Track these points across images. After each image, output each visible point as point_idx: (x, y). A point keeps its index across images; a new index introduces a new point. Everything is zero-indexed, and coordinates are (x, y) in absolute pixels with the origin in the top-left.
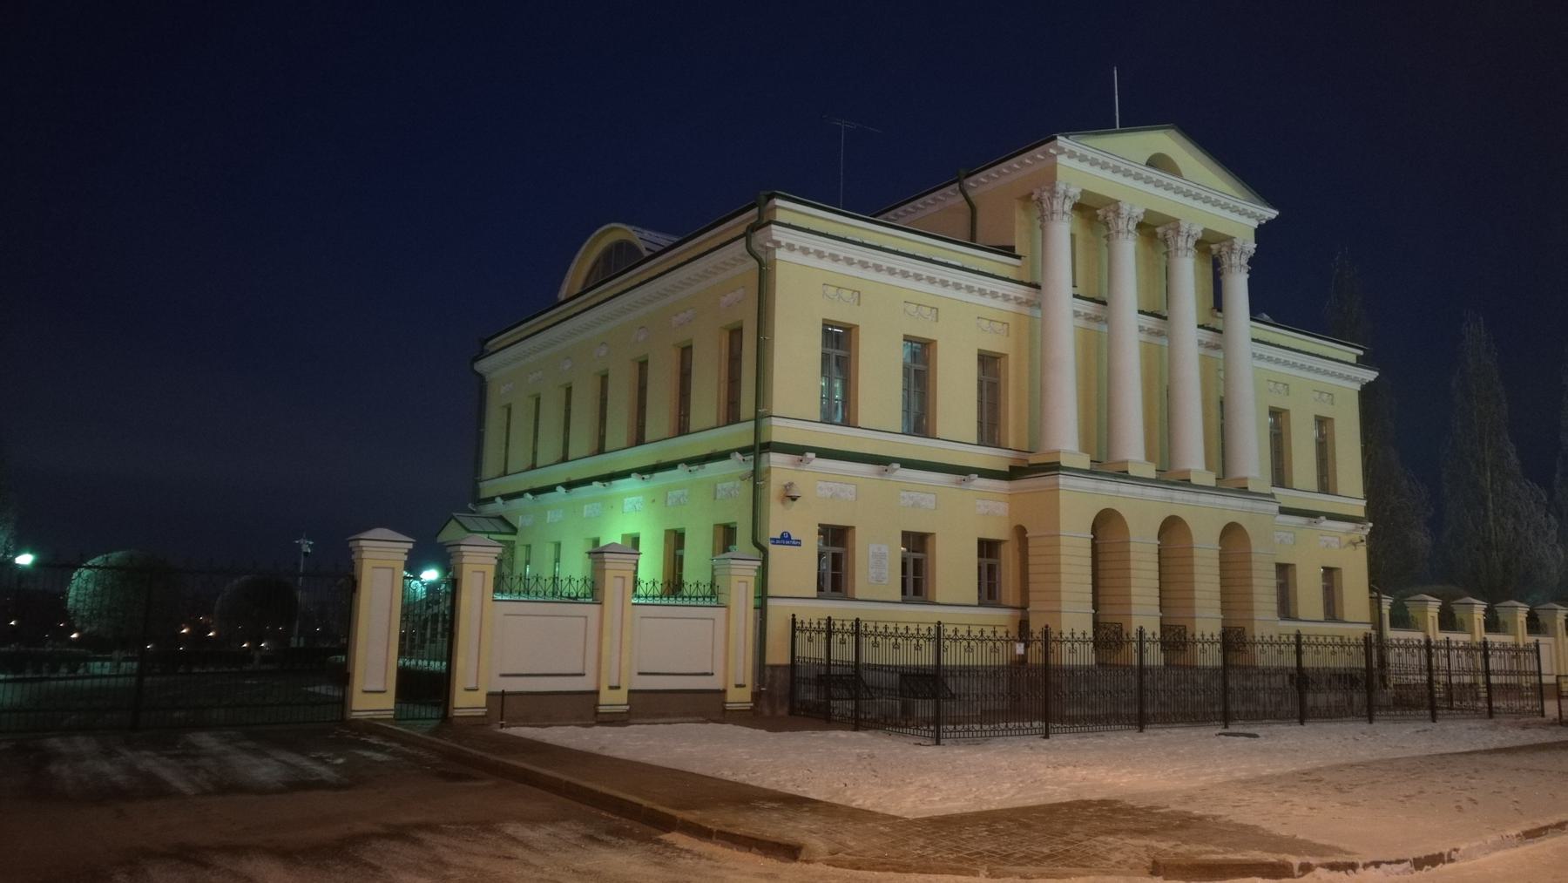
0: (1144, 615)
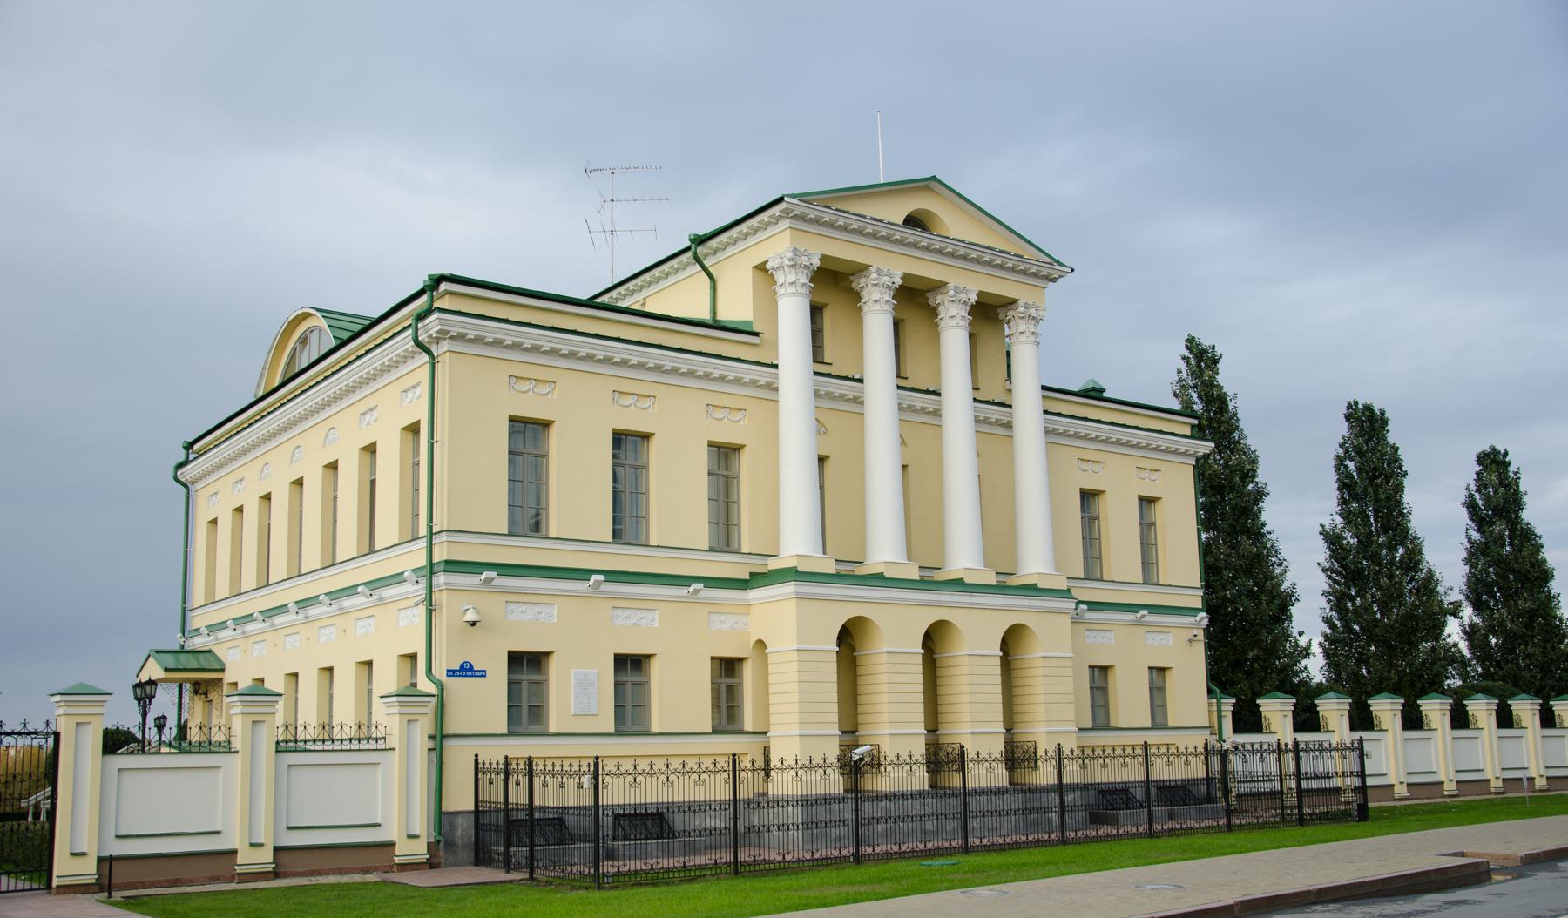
0: (895, 730)
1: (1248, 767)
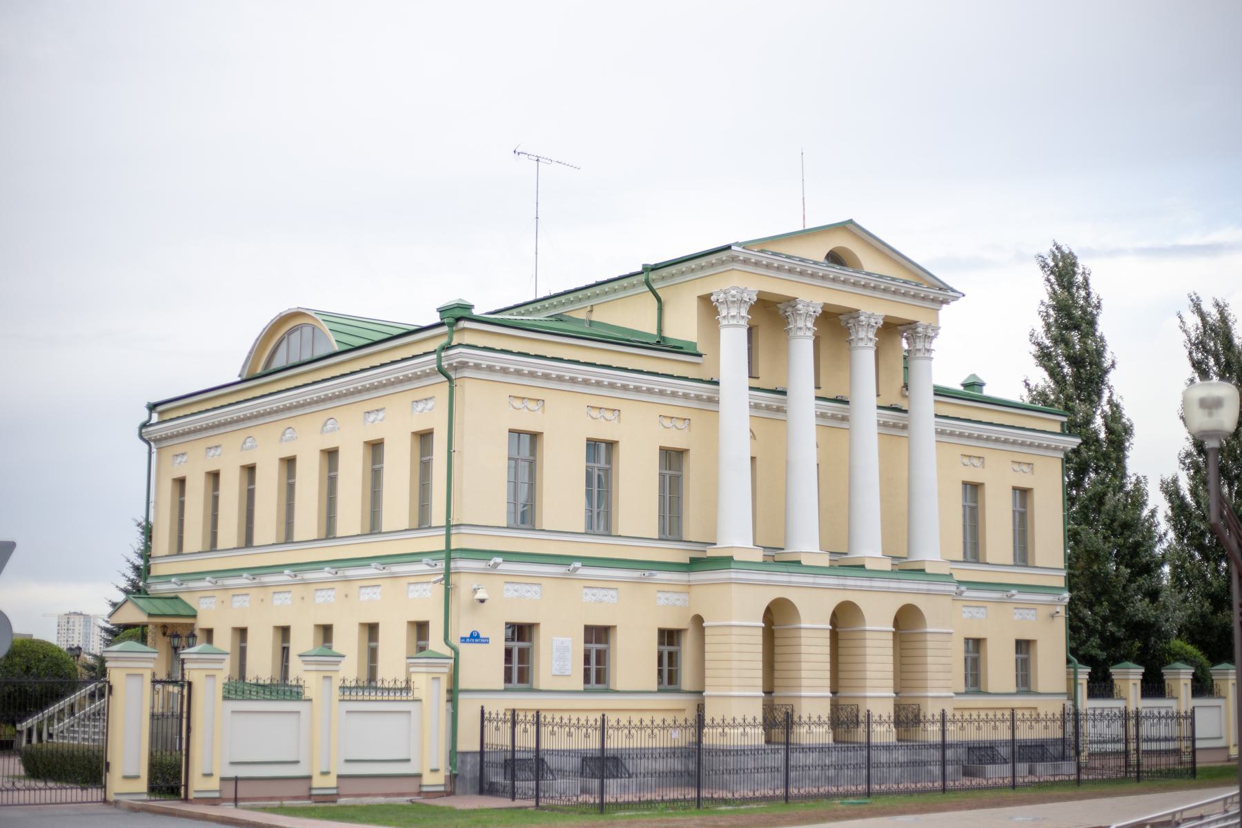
1: (1098, 730)
